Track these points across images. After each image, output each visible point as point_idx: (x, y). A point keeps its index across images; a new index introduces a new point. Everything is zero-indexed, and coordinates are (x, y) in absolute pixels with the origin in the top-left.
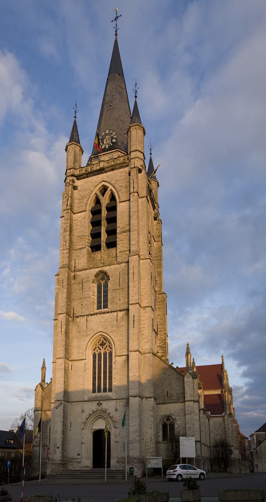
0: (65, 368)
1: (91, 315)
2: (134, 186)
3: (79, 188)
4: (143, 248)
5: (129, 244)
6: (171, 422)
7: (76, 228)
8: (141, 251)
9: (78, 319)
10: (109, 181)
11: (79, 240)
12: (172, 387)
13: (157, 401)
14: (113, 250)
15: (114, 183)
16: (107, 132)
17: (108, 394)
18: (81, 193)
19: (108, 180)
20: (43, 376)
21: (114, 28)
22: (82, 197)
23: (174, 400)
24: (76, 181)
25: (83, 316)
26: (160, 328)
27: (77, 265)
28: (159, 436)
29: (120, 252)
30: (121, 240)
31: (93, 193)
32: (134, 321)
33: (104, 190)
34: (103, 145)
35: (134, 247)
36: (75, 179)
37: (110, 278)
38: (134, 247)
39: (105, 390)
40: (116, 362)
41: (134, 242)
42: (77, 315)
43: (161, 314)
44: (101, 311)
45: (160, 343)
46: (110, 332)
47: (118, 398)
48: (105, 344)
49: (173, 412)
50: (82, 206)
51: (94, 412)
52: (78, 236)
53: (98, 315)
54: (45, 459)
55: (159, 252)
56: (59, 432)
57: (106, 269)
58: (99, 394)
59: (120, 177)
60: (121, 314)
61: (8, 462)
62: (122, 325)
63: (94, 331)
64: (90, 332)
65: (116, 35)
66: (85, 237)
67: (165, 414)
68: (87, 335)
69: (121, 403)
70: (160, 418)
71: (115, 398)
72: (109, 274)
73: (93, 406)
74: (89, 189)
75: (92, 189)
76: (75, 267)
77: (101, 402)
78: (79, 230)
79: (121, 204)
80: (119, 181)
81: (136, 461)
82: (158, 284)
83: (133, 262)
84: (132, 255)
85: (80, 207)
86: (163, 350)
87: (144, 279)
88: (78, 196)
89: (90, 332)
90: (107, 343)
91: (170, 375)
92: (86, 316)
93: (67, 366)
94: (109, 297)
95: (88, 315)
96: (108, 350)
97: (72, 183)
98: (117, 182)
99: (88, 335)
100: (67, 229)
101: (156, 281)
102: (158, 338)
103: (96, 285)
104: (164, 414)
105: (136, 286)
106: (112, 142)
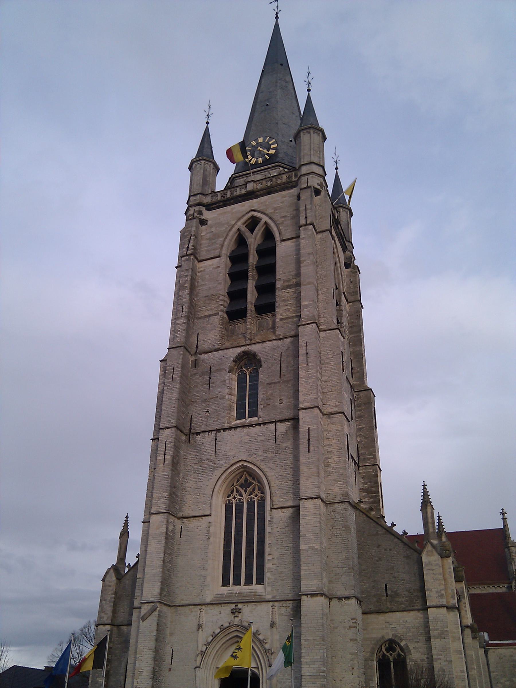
1: (225, 430)
7: (203, 283)
9: (199, 438)
11: (208, 302)
14: (268, 319)
15: (271, 213)
16: (261, 140)
17: (256, 588)
18: (213, 229)
19: (261, 208)
21: (274, 10)
25: (209, 432)
26: (363, 454)
27: (200, 343)
29: (281, 320)
30: (284, 300)
31: (235, 229)
32: (309, 440)
35: (307, 311)
36: (203, 209)
37: (263, 363)
38: (307, 311)
39: (249, 581)
42: (198, 430)
43: (363, 428)
44: (245, 422)
47: (277, 598)
49: (400, 632)
51: (223, 629)
52: (205, 297)
53: (238, 429)
55: (356, 319)
57: (254, 348)
58: (236, 589)
60: (282, 427)
62: (286, 447)
63: (230, 460)
64: (221, 462)
65: (277, 18)
66: (219, 297)
67: (383, 637)
69: (283, 610)
71: (269, 597)
75: (233, 222)
76: (197, 347)
77: (240, 606)
78: (208, 286)
79: (284, 243)
83: (306, 335)
84: (303, 323)
88: (208, 235)
89: (221, 462)
91: (390, 550)
92: (214, 433)
93: (171, 528)
94: (261, 396)
95: (218, 430)
96: (256, 496)
97: (198, 216)
98: (277, 211)
100: (185, 285)
102: (360, 473)
103: (235, 377)
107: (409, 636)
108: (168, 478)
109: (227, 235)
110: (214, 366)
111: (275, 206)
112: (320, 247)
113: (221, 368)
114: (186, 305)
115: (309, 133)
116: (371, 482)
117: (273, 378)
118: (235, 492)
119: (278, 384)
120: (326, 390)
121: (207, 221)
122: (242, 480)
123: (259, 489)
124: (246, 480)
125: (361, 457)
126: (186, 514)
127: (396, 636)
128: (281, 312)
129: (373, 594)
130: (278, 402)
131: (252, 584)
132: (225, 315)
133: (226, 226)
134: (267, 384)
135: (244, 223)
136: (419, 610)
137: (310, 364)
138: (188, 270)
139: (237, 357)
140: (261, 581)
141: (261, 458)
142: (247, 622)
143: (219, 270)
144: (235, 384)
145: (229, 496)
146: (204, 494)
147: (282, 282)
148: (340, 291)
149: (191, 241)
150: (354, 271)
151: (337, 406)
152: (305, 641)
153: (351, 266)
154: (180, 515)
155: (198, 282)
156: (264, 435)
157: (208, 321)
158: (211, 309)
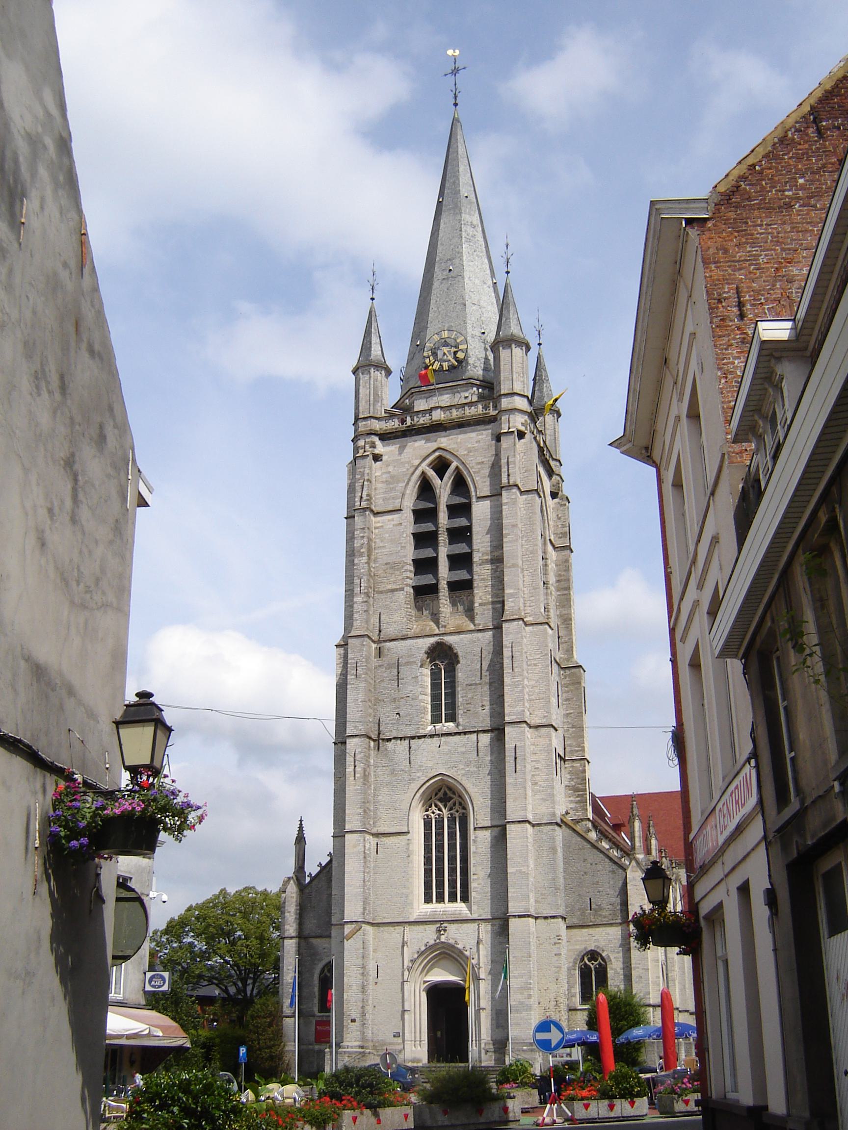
0: (365, 853)
1: (419, 737)
2: (508, 470)
3: (384, 458)
4: (531, 598)
5: (492, 561)
6: (600, 964)
7: (381, 545)
8: (528, 605)
9: (390, 745)
10: (453, 449)
11: (391, 571)
12: (601, 889)
13: (567, 922)
15: (464, 455)
18: (391, 469)
19: (451, 447)
20: (301, 857)
22: (392, 477)
23: (605, 917)
24: (378, 442)
25: (401, 739)
26: (570, 746)
27: (383, 626)
28: (574, 996)
29: (480, 605)
30: (482, 579)
31: (418, 473)
32: (516, 758)
33: (441, 466)
34: (436, 362)
35: (512, 602)
36: (376, 439)
37: (461, 659)
38: (512, 602)
40: (478, 839)
41: (511, 591)
42: (388, 735)
43: (571, 713)
45: (571, 779)
46: (463, 775)
48: (451, 798)
49: (602, 944)
50: (393, 498)
52: (386, 564)
54: (310, 1044)
55: (565, 571)
56: (354, 987)
58: (440, 907)
59: (476, 442)
61: (241, 1049)
64: (418, 775)
66: (403, 567)
67: (585, 948)
68: (412, 780)
70: (574, 956)
72: (460, 651)
73: (428, 935)
74: (408, 462)
75: (417, 462)
78: (388, 550)
80: (476, 450)
81: (525, 1048)
82: (563, 643)
83: (511, 633)
85: (389, 499)
86: (578, 796)
87: (535, 665)
88: (384, 476)
89: (418, 775)
90: (456, 798)
91: (596, 864)
92: (407, 741)
93: (367, 846)
94: (460, 700)
95: (413, 738)
96: (457, 811)
97: (370, 449)
98: (471, 454)
99: (414, 780)
100: (362, 551)
101: (559, 638)
102: (566, 768)
103: (427, 672)
104: (583, 947)
105: (518, 685)
106: (456, 358)
107: (611, 947)
108: (361, 793)
109: (409, 480)
110: (402, 657)
111: (470, 446)
112: (525, 512)
113: (412, 660)
114: (365, 578)
115: (510, 347)
116: (578, 778)
117: (473, 678)
118: (433, 805)
119: (479, 686)
120: (533, 697)
121: (382, 455)
122: (441, 794)
123: (460, 804)
124: (445, 794)
125: (568, 749)
126: (381, 830)
127: (598, 947)
128: (480, 594)
129: (577, 908)
130: (481, 708)
131: (456, 901)
132: (412, 591)
133: (406, 465)
134: (467, 685)
135: (430, 464)
136: (621, 924)
137: (516, 670)
138: (364, 529)
139: (429, 648)
140: (465, 898)
141: (463, 772)
142: (453, 939)
143: (401, 528)
144: (428, 680)
145: (427, 810)
146: (400, 809)
147: (480, 555)
148: (545, 538)
149: (365, 489)
150: (563, 503)
151: (545, 717)
152: (513, 957)
153: (559, 496)
154: (374, 831)
155: (375, 542)
156: (464, 746)
157: (391, 598)
158: (394, 582)
